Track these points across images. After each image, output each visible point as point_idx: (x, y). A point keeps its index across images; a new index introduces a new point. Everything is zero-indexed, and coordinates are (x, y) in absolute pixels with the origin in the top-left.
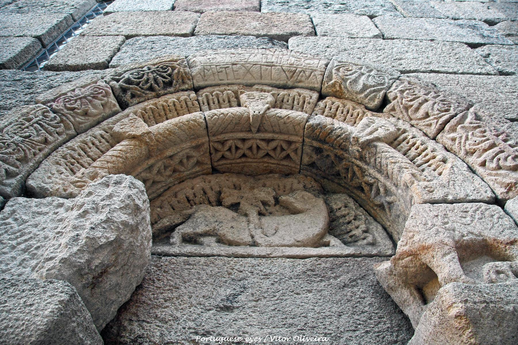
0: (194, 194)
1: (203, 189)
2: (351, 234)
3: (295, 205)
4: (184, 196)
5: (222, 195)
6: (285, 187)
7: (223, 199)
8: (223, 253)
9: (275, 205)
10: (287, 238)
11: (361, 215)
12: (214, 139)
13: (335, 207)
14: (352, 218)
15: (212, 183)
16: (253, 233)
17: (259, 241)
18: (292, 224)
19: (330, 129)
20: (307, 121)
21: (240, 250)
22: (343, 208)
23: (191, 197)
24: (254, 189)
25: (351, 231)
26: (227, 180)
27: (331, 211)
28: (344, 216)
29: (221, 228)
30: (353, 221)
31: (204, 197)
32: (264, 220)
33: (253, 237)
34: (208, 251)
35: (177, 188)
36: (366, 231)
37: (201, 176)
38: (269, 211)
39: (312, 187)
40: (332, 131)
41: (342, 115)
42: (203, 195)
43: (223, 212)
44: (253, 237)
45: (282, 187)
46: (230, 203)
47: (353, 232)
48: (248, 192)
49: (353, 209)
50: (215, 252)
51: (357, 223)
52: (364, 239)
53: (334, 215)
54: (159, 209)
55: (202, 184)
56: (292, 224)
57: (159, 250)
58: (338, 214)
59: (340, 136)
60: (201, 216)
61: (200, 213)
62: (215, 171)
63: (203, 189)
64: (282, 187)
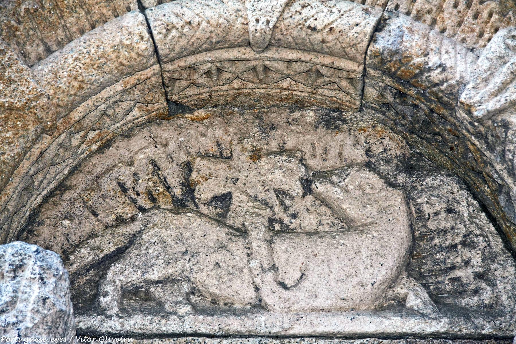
0: (135, 175)
1: (153, 162)
2: (452, 275)
3: (344, 206)
4: (114, 183)
5: (194, 175)
6: (326, 151)
7: (197, 183)
8: (203, 329)
9: (304, 195)
10: (323, 293)
11: (477, 236)
12: (169, 67)
13: (427, 209)
14: (459, 239)
15: (172, 147)
16: (258, 281)
17: (269, 300)
18: (334, 259)
19: (418, 67)
20: (373, 39)
21: (234, 324)
22: (443, 215)
23: (129, 184)
24: (259, 158)
25: (453, 267)
26: (203, 135)
27: (417, 218)
28: (444, 231)
29: (195, 268)
30: (460, 247)
31: (156, 178)
32: (281, 246)
33: (257, 289)
34: (173, 325)
35: (98, 164)
36: (480, 276)
37: (146, 131)
38: (291, 211)
39: (385, 150)
40: (422, 73)
41: (455, 11)
42: (153, 173)
43: (197, 229)
44: (257, 289)
45: (319, 151)
46: (210, 196)
47: (458, 273)
48: (246, 165)
49: (462, 217)
50: (188, 329)
51: (467, 254)
52: (476, 292)
53: (425, 226)
54: (66, 222)
55: (151, 152)
56: (334, 259)
57: (81, 324)
58: (431, 225)
59: (437, 85)
60: (155, 239)
61: (152, 232)
62: (176, 109)
63: (153, 162)
64: (319, 151)
